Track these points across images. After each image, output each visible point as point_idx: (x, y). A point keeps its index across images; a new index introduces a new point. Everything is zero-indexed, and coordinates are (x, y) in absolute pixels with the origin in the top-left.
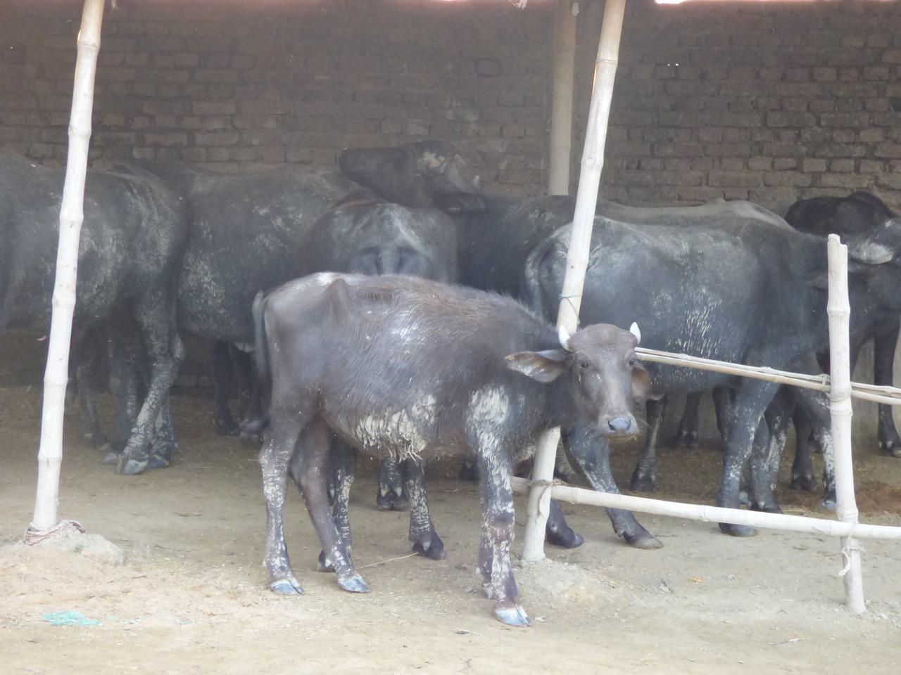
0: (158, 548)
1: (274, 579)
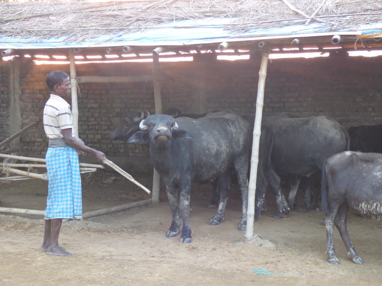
0: (286, 244)
1: (330, 258)
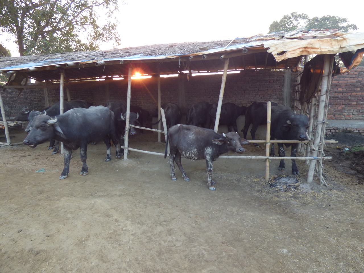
1: (172, 178)
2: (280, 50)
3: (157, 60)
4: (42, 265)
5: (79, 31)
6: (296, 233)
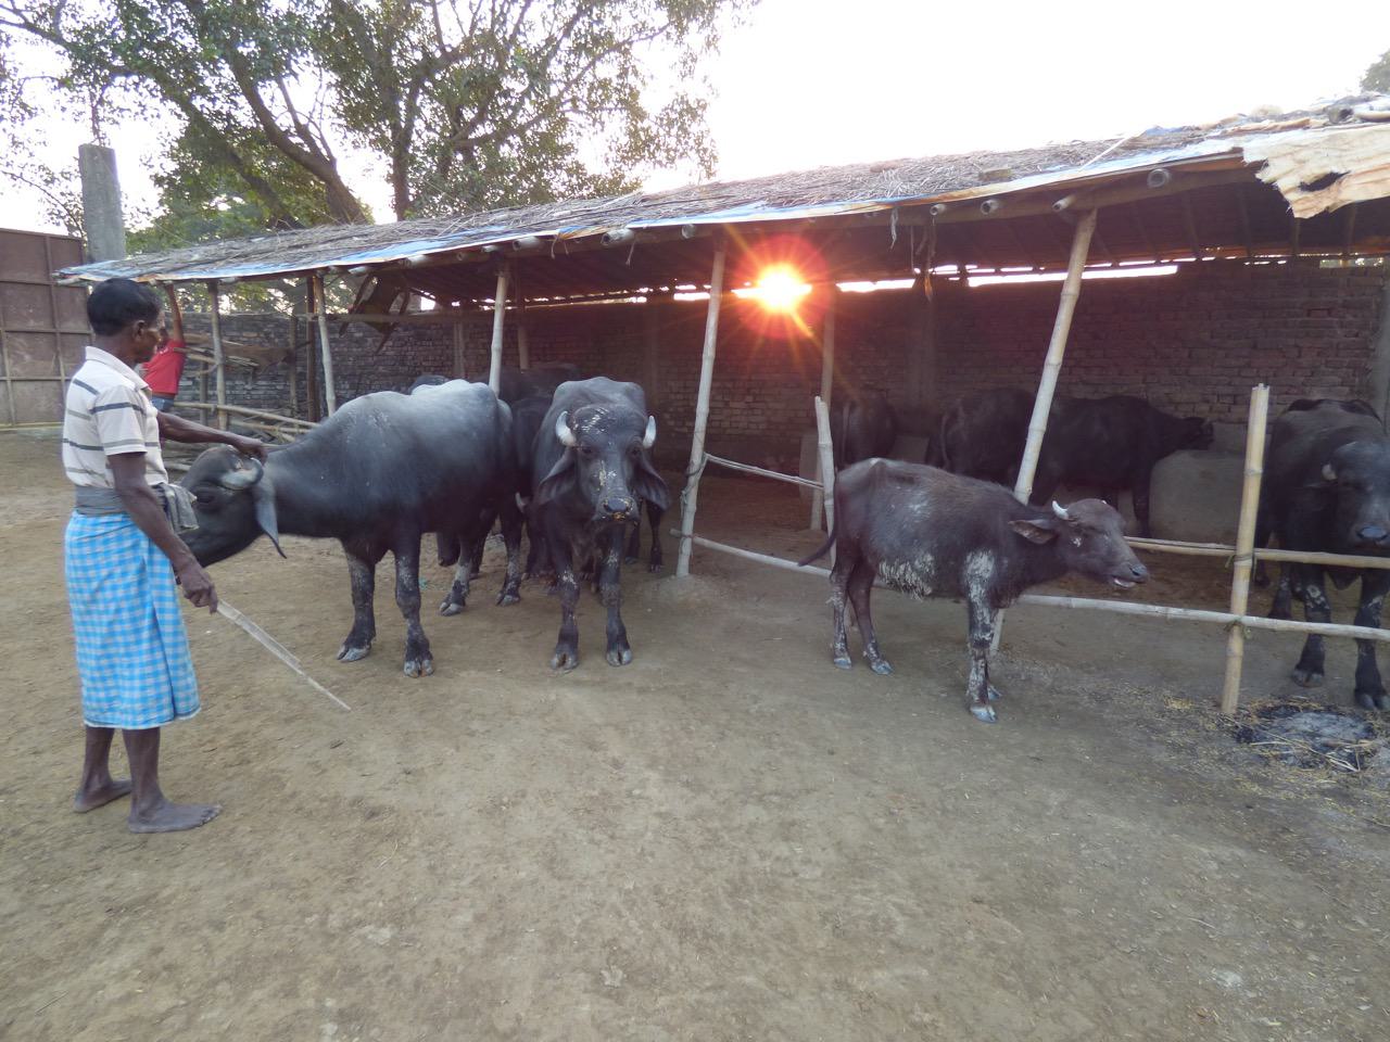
1: (837, 657)
2: (1315, 170)
3: (811, 221)
4: (383, 847)
5: (579, 134)
6: (1306, 929)
